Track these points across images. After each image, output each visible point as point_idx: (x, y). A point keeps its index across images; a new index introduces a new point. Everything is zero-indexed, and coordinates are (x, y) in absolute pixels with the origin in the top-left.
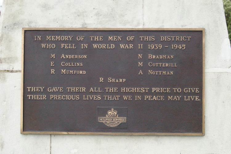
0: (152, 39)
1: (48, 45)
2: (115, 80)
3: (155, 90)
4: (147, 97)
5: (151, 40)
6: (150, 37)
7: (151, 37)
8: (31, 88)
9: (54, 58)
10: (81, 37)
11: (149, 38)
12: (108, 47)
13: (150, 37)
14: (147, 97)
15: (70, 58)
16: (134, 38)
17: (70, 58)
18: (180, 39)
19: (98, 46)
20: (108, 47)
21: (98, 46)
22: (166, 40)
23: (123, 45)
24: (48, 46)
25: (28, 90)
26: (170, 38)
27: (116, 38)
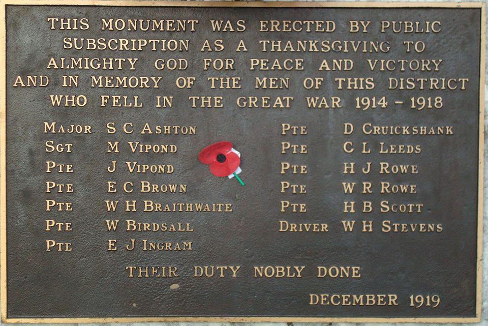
0: (409, 85)
1: (67, 96)
2: (428, 130)
3: (257, 64)
4: (258, 61)
5: (364, 86)
6: (361, 79)
7: (364, 81)
8: (297, 205)
9: (117, 151)
10: (187, 80)
11: (358, 82)
12: (188, 227)
13: (361, 79)
14: (258, 61)
15: (169, 172)
16: (194, 81)
17: (169, 172)
18: (440, 84)
19: (156, 168)
20: (188, 227)
21: (156, 168)
22: (402, 88)
23: (219, 23)
24: (67, 100)
25: (293, 208)
26: (413, 82)
27: (112, 80)
